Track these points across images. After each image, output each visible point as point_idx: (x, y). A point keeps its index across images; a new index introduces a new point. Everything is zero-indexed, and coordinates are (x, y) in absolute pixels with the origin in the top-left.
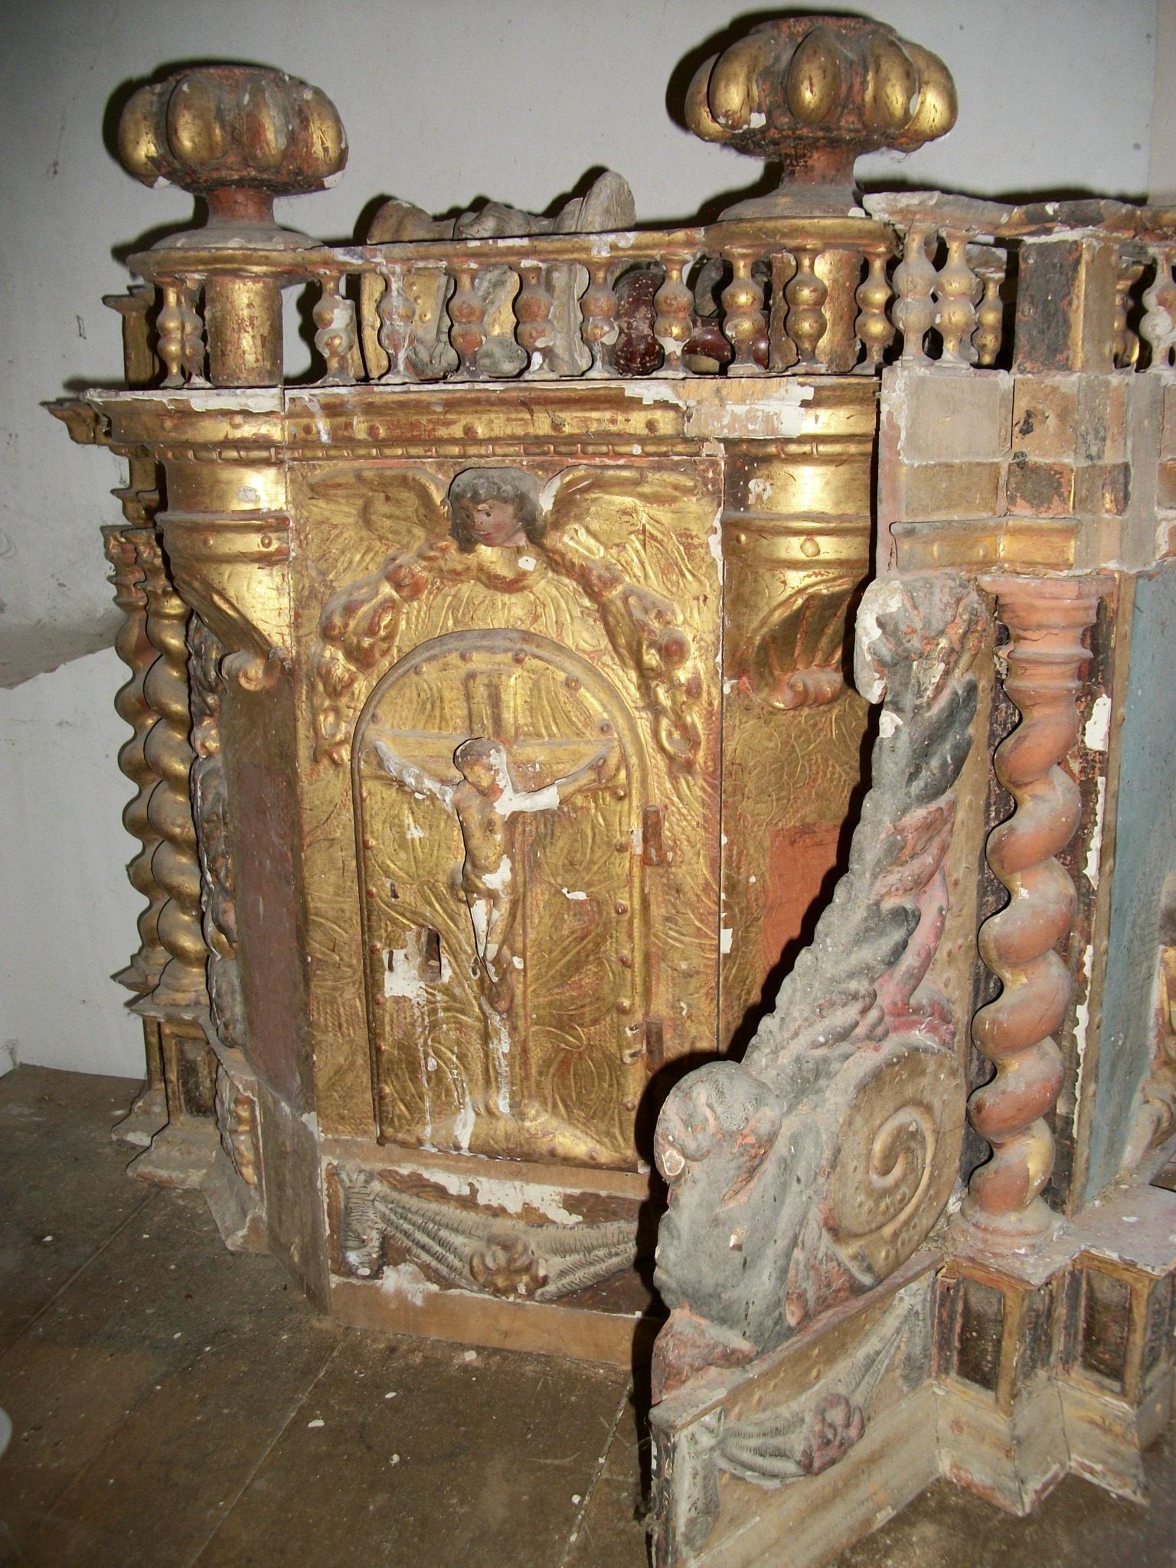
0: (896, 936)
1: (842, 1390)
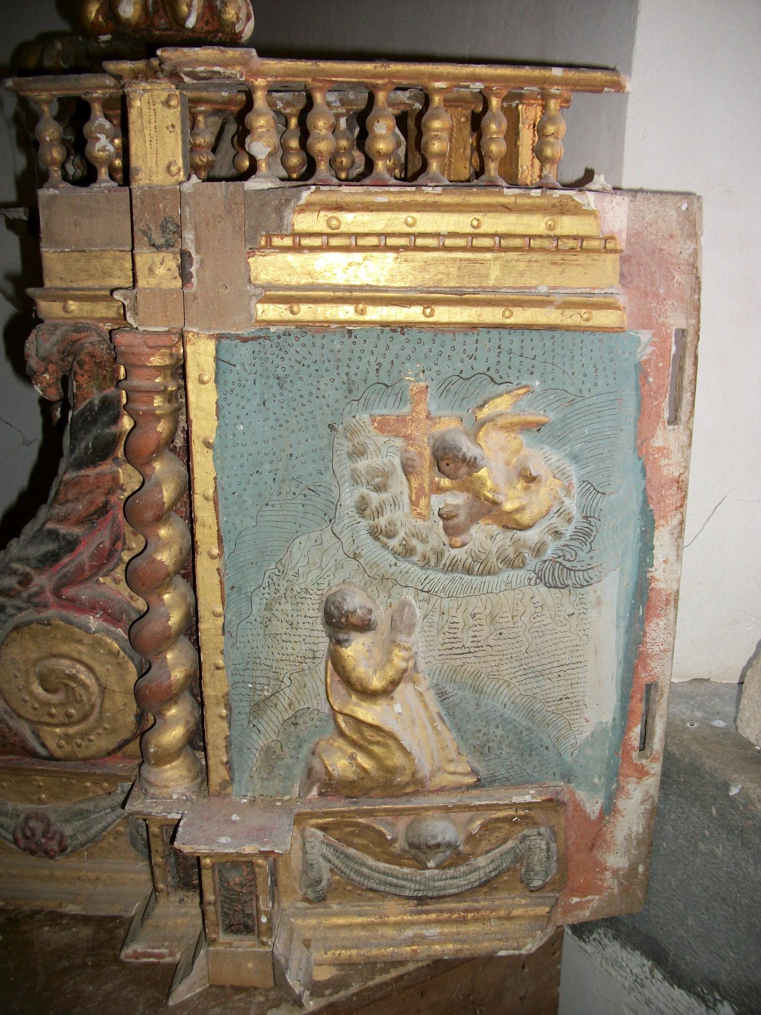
0: (51, 546)
1: (53, 817)
